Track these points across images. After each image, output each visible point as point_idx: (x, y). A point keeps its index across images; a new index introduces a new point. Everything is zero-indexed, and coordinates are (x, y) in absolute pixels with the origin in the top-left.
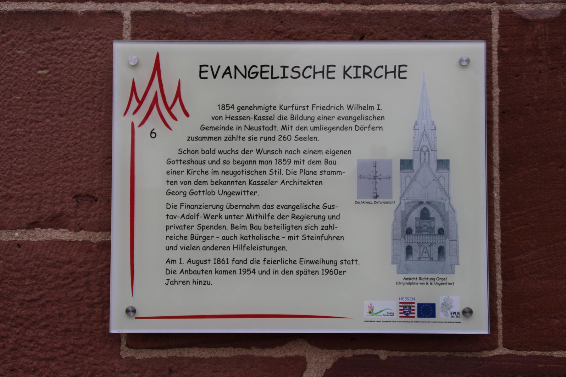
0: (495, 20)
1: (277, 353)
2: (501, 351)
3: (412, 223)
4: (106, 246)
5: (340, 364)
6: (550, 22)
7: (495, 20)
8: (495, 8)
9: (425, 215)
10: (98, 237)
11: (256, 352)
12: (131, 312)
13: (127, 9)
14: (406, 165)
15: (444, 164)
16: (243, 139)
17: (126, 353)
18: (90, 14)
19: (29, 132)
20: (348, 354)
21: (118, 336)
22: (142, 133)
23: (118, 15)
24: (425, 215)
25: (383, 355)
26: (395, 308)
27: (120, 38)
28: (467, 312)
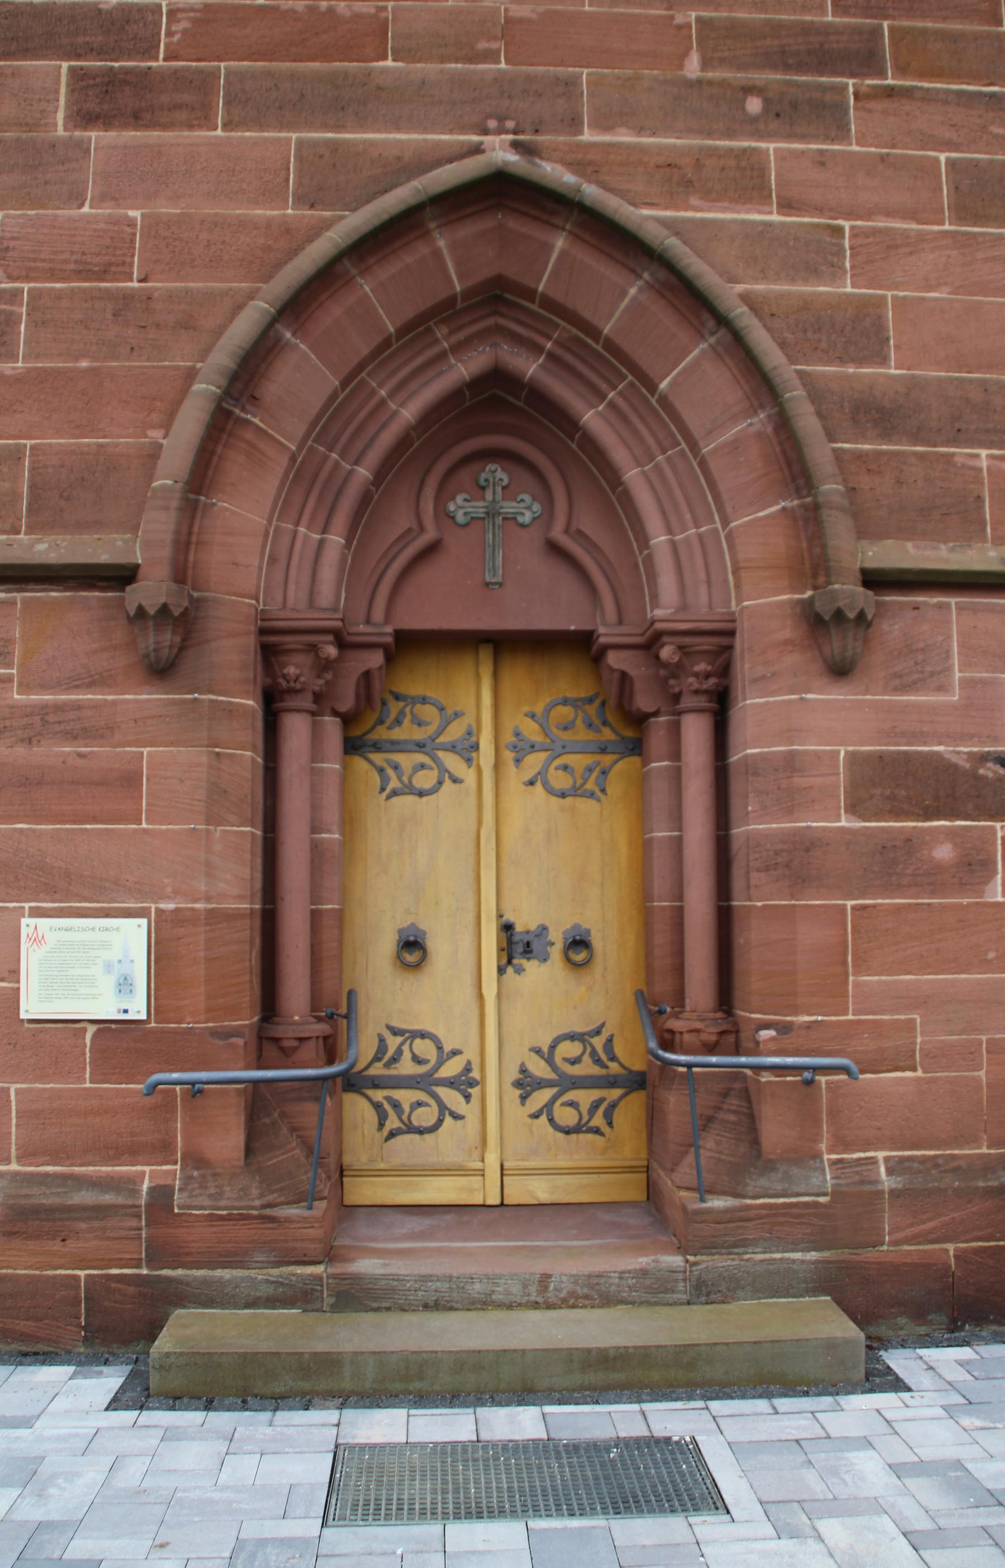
0: (153, 910)
1: (77, 1026)
2: (153, 1025)
3: (121, 981)
4: (19, 989)
5: (99, 1030)
6: (172, 911)
7: (153, 910)
8: (153, 906)
9: (126, 979)
10: (16, 985)
11: (70, 1025)
12: (27, 1011)
13: (27, 905)
14: (120, 961)
15: (132, 961)
16: (93, 929)
17: (26, 1025)
18: (14, 908)
19: (164, 610)
20: (102, 1026)
21: (23, 1020)
22: (31, 950)
23: (23, 908)
24: (126, 979)
25: (113, 1026)
26: (115, 1011)
27: (24, 916)
28: (139, 1012)
